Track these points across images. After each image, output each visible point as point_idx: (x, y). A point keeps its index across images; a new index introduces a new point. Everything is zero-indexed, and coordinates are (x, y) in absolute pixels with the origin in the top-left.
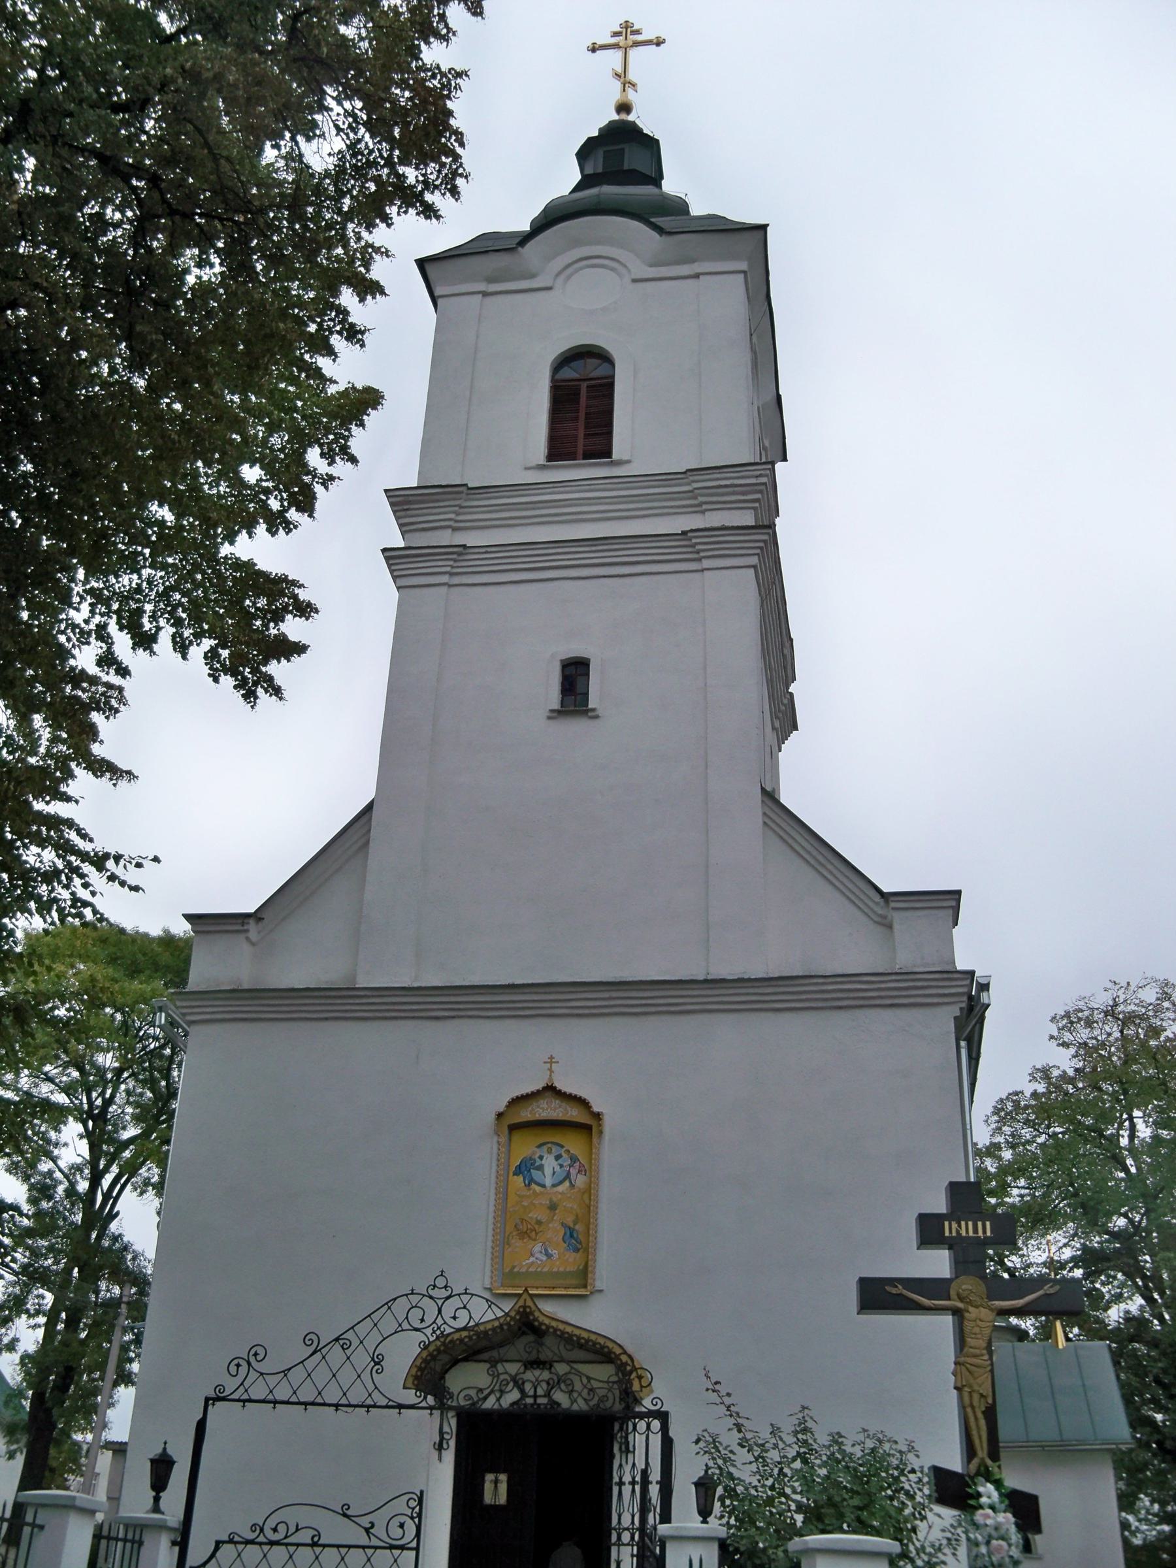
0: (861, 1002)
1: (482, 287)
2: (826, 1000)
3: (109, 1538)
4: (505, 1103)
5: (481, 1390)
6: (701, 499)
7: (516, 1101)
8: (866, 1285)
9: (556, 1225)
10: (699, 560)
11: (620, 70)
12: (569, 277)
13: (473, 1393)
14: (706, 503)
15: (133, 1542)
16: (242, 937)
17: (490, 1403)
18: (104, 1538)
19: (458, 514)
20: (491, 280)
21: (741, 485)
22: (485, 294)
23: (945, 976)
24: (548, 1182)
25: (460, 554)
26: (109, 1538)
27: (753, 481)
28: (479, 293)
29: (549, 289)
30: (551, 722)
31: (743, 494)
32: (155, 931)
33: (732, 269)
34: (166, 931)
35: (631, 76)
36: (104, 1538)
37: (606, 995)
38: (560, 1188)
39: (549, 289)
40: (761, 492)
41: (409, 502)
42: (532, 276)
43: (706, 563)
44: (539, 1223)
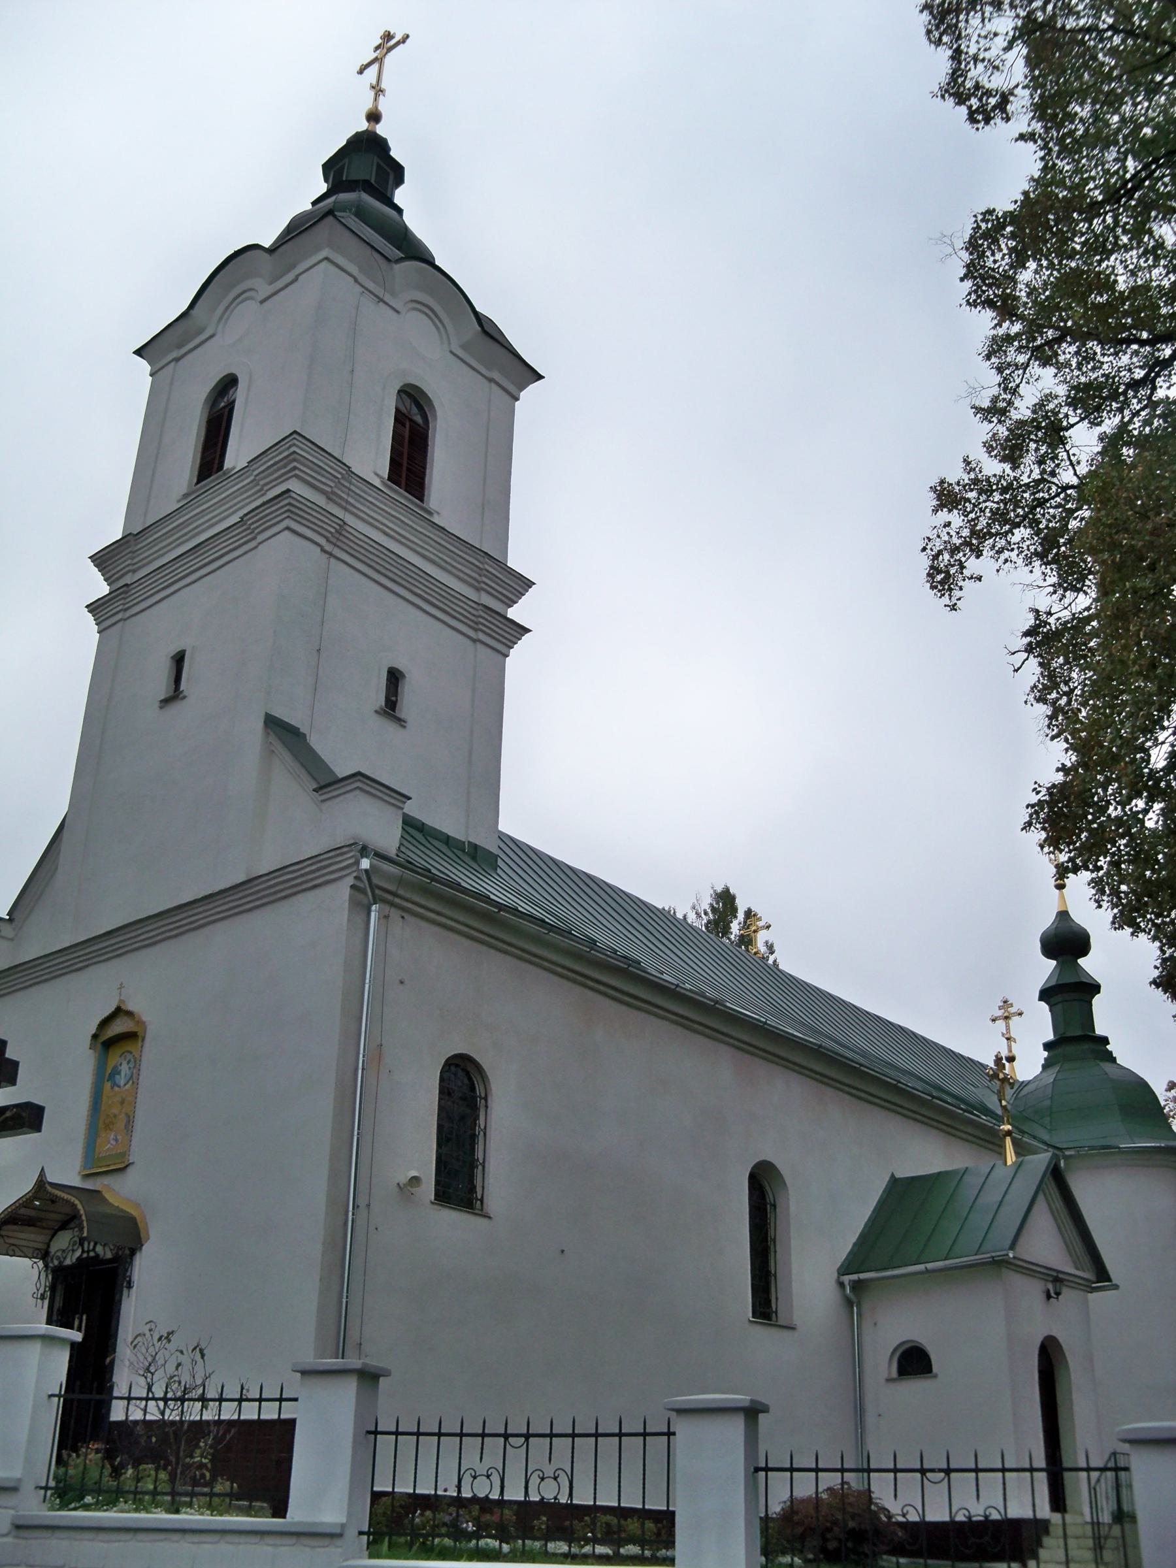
1: (174, 355)
2: (275, 893)
3: (767, 1469)
5: (63, 1251)
6: (262, 483)
8: (36, 1126)
9: (122, 1116)
10: (254, 538)
11: (374, 83)
12: (228, 319)
13: (59, 1254)
15: (757, 1470)
17: (68, 1262)
18: (762, 1469)
19: (133, 558)
20: (179, 346)
21: (281, 460)
22: (177, 360)
23: (338, 852)
24: (122, 1083)
25: (126, 592)
26: (767, 1469)
27: (286, 454)
28: (170, 362)
29: (398, 312)
31: (285, 466)
32: (660, 907)
35: (383, 86)
36: (762, 1469)
37: (438, 908)
38: (127, 1087)
39: (398, 312)
40: (294, 460)
41: (105, 561)
43: (260, 538)
44: (115, 1116)
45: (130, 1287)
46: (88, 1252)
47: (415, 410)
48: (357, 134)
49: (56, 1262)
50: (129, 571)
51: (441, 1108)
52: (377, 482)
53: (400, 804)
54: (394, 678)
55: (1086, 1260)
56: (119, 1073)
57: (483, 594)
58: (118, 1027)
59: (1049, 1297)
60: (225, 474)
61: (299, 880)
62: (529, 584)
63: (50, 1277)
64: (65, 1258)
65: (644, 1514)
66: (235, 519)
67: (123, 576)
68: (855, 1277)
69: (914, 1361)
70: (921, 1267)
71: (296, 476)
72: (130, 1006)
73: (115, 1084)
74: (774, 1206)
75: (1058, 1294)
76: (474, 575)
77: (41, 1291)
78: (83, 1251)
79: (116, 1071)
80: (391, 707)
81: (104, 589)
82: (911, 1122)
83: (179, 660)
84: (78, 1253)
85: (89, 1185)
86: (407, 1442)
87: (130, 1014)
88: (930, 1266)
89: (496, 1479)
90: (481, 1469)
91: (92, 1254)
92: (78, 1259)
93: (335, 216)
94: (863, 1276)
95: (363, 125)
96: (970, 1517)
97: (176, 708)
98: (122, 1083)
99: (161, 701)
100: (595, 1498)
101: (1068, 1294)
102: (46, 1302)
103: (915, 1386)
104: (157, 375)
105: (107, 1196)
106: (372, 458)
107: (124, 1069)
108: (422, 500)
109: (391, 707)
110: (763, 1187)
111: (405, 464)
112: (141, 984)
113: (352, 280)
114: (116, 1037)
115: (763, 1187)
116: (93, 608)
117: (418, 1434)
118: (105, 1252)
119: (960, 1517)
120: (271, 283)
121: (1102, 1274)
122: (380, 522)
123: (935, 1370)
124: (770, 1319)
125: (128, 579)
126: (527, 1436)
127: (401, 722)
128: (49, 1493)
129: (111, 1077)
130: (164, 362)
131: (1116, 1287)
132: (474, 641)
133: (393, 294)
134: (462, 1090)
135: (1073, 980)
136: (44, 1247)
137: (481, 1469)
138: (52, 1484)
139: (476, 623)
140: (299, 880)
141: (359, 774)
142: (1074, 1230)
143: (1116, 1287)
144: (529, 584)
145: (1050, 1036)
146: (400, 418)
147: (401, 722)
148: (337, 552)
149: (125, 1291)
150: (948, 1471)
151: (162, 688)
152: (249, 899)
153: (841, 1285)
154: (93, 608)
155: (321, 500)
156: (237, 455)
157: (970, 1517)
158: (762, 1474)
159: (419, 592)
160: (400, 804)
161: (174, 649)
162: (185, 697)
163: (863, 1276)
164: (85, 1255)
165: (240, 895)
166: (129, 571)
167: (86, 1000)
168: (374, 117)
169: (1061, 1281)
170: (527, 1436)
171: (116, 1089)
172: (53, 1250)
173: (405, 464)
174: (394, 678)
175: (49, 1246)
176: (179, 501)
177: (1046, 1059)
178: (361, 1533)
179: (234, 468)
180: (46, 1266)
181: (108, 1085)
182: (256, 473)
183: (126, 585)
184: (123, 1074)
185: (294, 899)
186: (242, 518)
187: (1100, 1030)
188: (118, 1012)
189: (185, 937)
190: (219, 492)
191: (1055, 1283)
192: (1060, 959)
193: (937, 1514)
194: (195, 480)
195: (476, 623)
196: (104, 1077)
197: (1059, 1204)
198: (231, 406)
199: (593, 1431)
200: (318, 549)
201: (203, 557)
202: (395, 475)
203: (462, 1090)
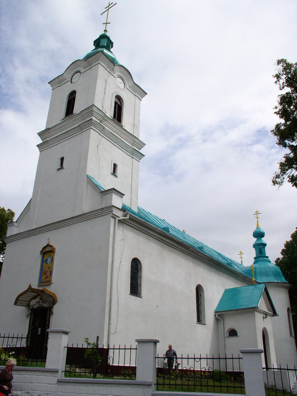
0: (96, 217)
1: (59, 85)
4: (42, 249)
5: (34, 305)
6: (84, 117)
7: (44, 248)
9: (49, 271)
13: (33, 305)
14: (85, 117)
15: (156, 358)
16: (13, 226)
17: (35, 307)
18: (157, 358)
22: (59, 86)
29: (115, 78)
30: (58, 171)
33: (96, 64)
34: (291, 237)
36: (157, 358)
39: (115, 78)
41: (41, 135)
42: (66, 79)
43: (84, 130)
44: (47, 271)
45: (52, 314)
46: (41, 305)
47: (118, 102)
48: (100, 36)
49: (32, 307)
50: (48, 137)
52: (111, 118)
53: (122, 196)
54: (115, 166)
55: (271, 309)
56: (48, 261)
57: (134, 147)
58: (48, 249)
59: (264, 318)
60: (73, 114)
61: (97, 214)
62: (145, 145)
63: (30, 311)
64: (34, 306)
65: (130, 367)
66: (77, 125)
67: (46, 138)
69: (233, 333)
71: (93, 115)
72: (51, 244)
73: (46, 263)
74: (201, 295)
75: (266, 317)
76: (132, 142)
77: (28, 314)
78: (39, 305)
79: (47, 260)
81: (41, 141)
82: (229, 276)
83: (62, 159)
84: (38, 305)
85: (41, 288)
86: (122, 351)
87: (51, 246)
91: (42, 306)
92: (38, 307)
95: (103, 33)
97: (61, 171)
98: (49, 263)
99: (58, 169)
100: (226, 370)
101: (268, 318)
102: (29, 317)
103: (233, 339)
104: (53, 90)
105: (45, 291)
106: (110, 113)
107: (49, 259)
110: (199, 290)
112: (54, 239)
113: (105, 69)
115: (199, 290)
116: (38, 146)
118: (46, 305)
120: (84, 69)
122: (110, 127)
123: (238, 335)
124: (199, 322)
125: (48, 139)
127: (116, 176)
129: (46, 261)
130: (56, 87)
133: (114, 73)
134: (136, 265)
135: (261, 243)
139: (133, 153)
140: (97, 214)
141: (114, 189)
142: (269, 303)
144: (145, 145)
145: (255, 256)
146: (116, 103)
147: (116, 176)
149: (51, 315)
150: (200, 359)
151: (59, 167)
152: (84, 218)
154: (38, 146)
156: (77, 109)
158: (157, 359)
159: (120, 145)
160: (122, 196)
162: (64, 168)
164: (40, 306)
165: (81, 217)
166: (48, 137)
167: (40, 242)
168: (105, 31)
169: (267, 314)
171: (47, 264)
174: (115, 166)
176: (61, 121)
177: (254, 261)
178: (63, 371)
179: (76, 113)
180: (29, 309)
181: (45, 264)
182: (82, 114)
183: (48, 141)
184: (49, 261)
185: (96, 219)
186: (79, 125)
187: (267, 255)
188: (48, 245)
189: (65, 227)
190: (70, 120)
192: (258, 238)
193: (197, 368)
194: (65, 116)
195: (133, 153)
196: (44, 261)
198: (74, 98)
199: (130, 348)
200: (98, 134)
201: (68, 135)
202: (114, 117)
203: (136, 265)
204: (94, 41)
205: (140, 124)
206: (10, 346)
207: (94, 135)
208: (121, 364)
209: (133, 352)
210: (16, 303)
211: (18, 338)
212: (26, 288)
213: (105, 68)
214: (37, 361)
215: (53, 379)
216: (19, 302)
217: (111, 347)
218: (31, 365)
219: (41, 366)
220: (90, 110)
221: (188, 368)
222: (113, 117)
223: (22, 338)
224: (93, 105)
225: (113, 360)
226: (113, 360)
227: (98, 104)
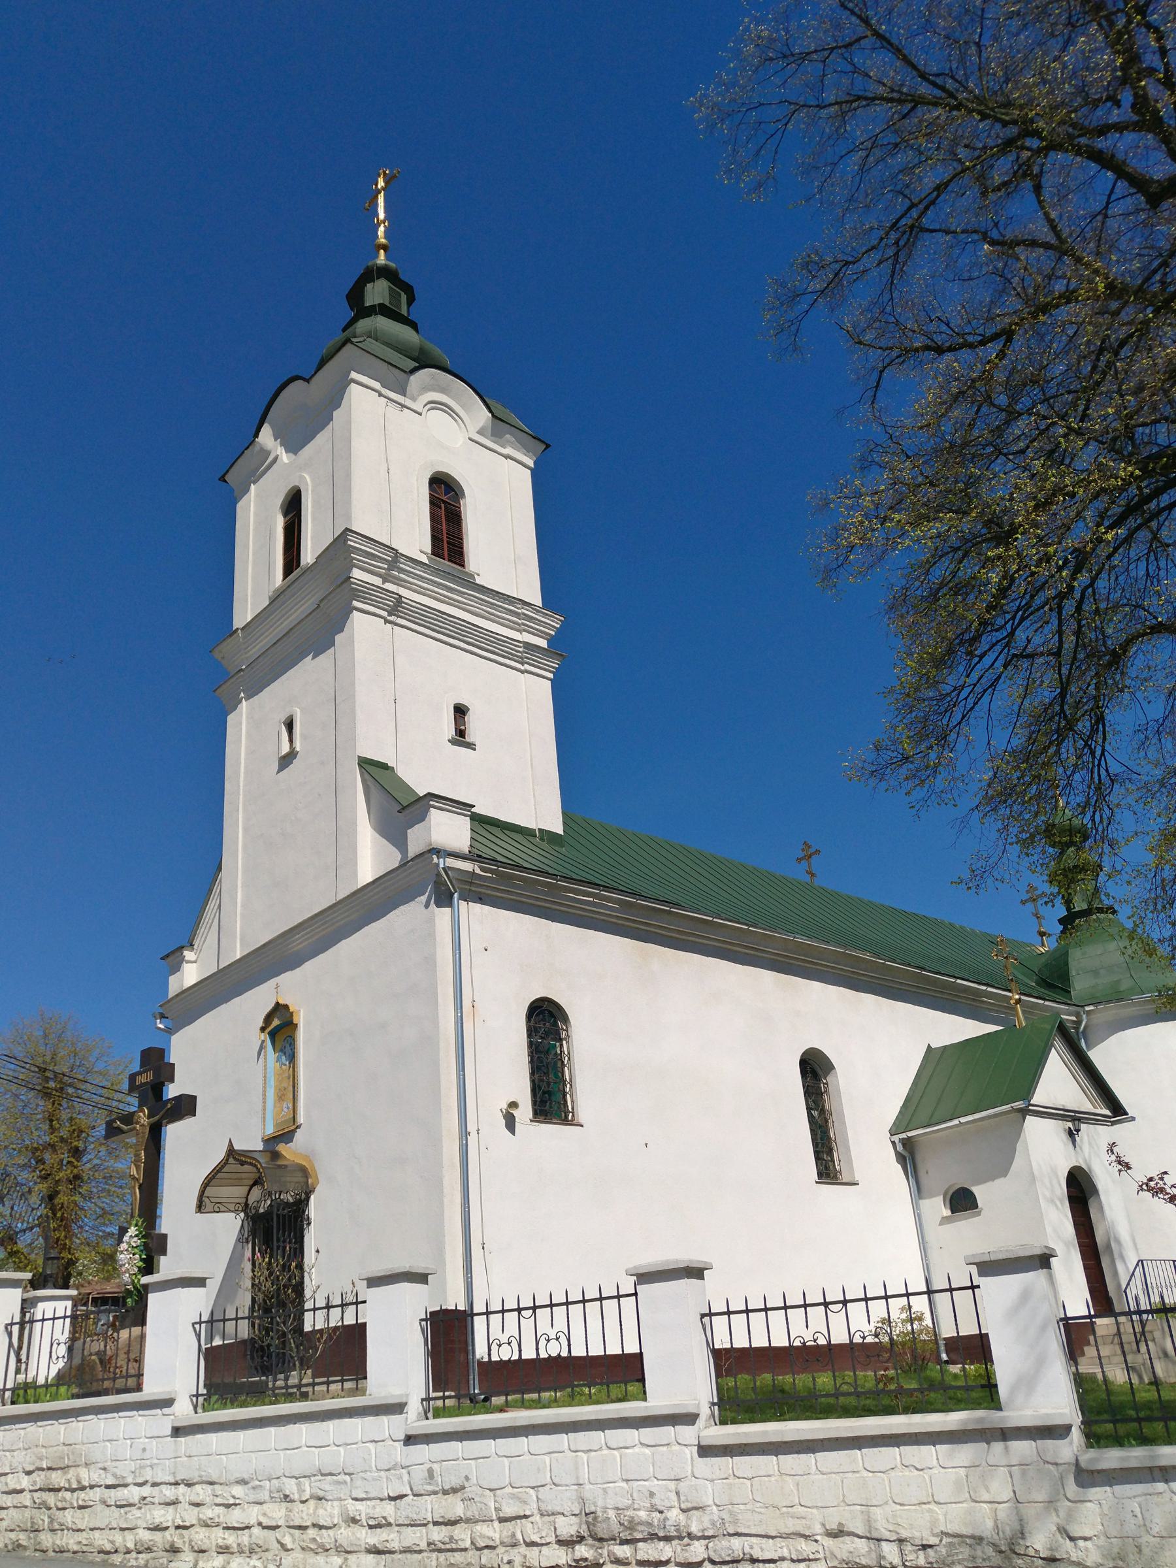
4: (261, 1020)
7: (268, 1018)
17: (261, 1211)
49: (253, 1211)
51: (530, 1044)
52: (425, 559)
54: (460, 711)
68: (904, 1136)
70: (956, 1122)
75: (1078, 1131)
80: (460, 737)
84: (269, 1202)
86: (560, 1311)
88: (963, 1120)
89: (515, 1345)
90: (504, 1339)
93: (352, 343)
94: (910, 1134)
96: (804, 1343)
106: (414, 537)
108: (463, 566)
109: (460, 737)
110: (814, 1069)
111: (445, 539)
114: (280, 1027)
115: (814, 1069)
117: (747, 1311)
119: (797, 1343)
121: (1117, 1110)
123: (980, 1205)
126: (845, 1302)
127: (471, 746)
128: (201, 1399)
131: (1133, 1119)
132: (522, 672)
133: (414, 399)
136: (244, 1200)
137: (504, 1339)
138: (203, 1391)
143: (1133, 1119)
147: (471, 746)
148: (400, 621)
153: (893, 1143)
155: (378, 581)
156: (309, 555)
157: (804, 1343)
161: (283, 717)
163: (910, 1134)
170: (845, 1302)
172: (250, 1202)
173: (445, 539)
175: (247, 1199)
191: (1073, 1120)
193: (839, 1337)
197: (1068, 1057)
202: (437, 551)
204: (347, 296)
205: (229, 640)
206: (864, 1338)
207: (365, 629)
208: (596, 1350)
209: (628, 1304)
210: (200, 1208)
211: (519, 1310)
212: (221, 1155)
213: (373, 390)
214: (328, 1383)
215: (161, 1422)
216: (208, 1205)
217: (479, 1307)
218: (327, 1395)
219: (358, 1391)
220: (342, 546)
221: (808, 1337)
222: (429, 550)
223: (534, 1308)
224: (347, 530)
225: (569, 1341)
226: (569, 1341)
227: (366, 522)
